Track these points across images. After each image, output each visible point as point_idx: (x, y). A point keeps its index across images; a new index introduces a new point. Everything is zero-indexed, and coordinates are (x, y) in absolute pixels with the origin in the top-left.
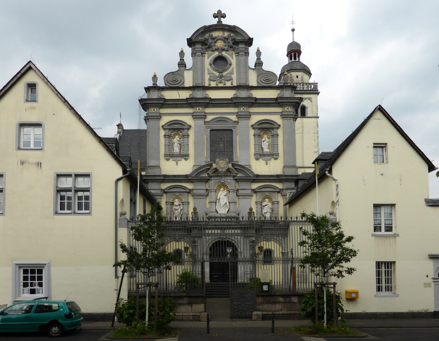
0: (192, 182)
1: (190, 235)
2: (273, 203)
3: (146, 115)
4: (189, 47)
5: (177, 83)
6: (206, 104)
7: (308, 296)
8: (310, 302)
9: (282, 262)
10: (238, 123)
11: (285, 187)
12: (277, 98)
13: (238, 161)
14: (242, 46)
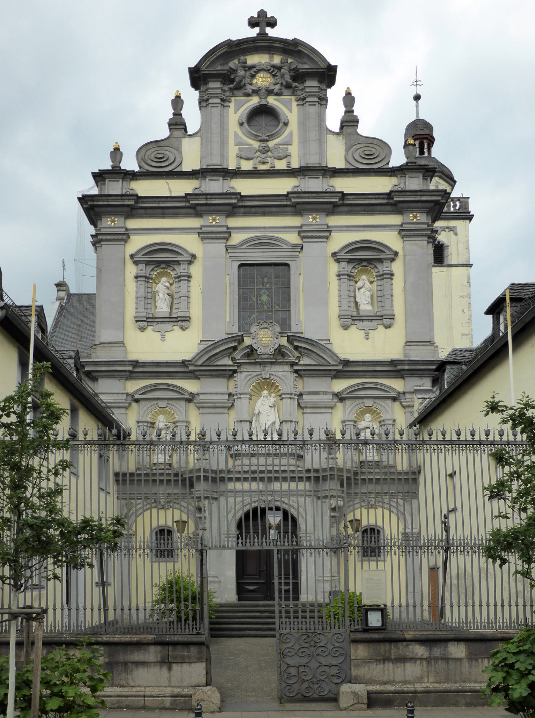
0: (197, 378)
1: (191, 493)
2: (383, 423)
3: (93, 232)
4: (193, 89)
5: (166, 164)
6: (230, 208)
8: (517, 666)
10: (302, 249)
11: (409, 388)
12: (391, 192)
13: (301, 331)
14: (312, 84)
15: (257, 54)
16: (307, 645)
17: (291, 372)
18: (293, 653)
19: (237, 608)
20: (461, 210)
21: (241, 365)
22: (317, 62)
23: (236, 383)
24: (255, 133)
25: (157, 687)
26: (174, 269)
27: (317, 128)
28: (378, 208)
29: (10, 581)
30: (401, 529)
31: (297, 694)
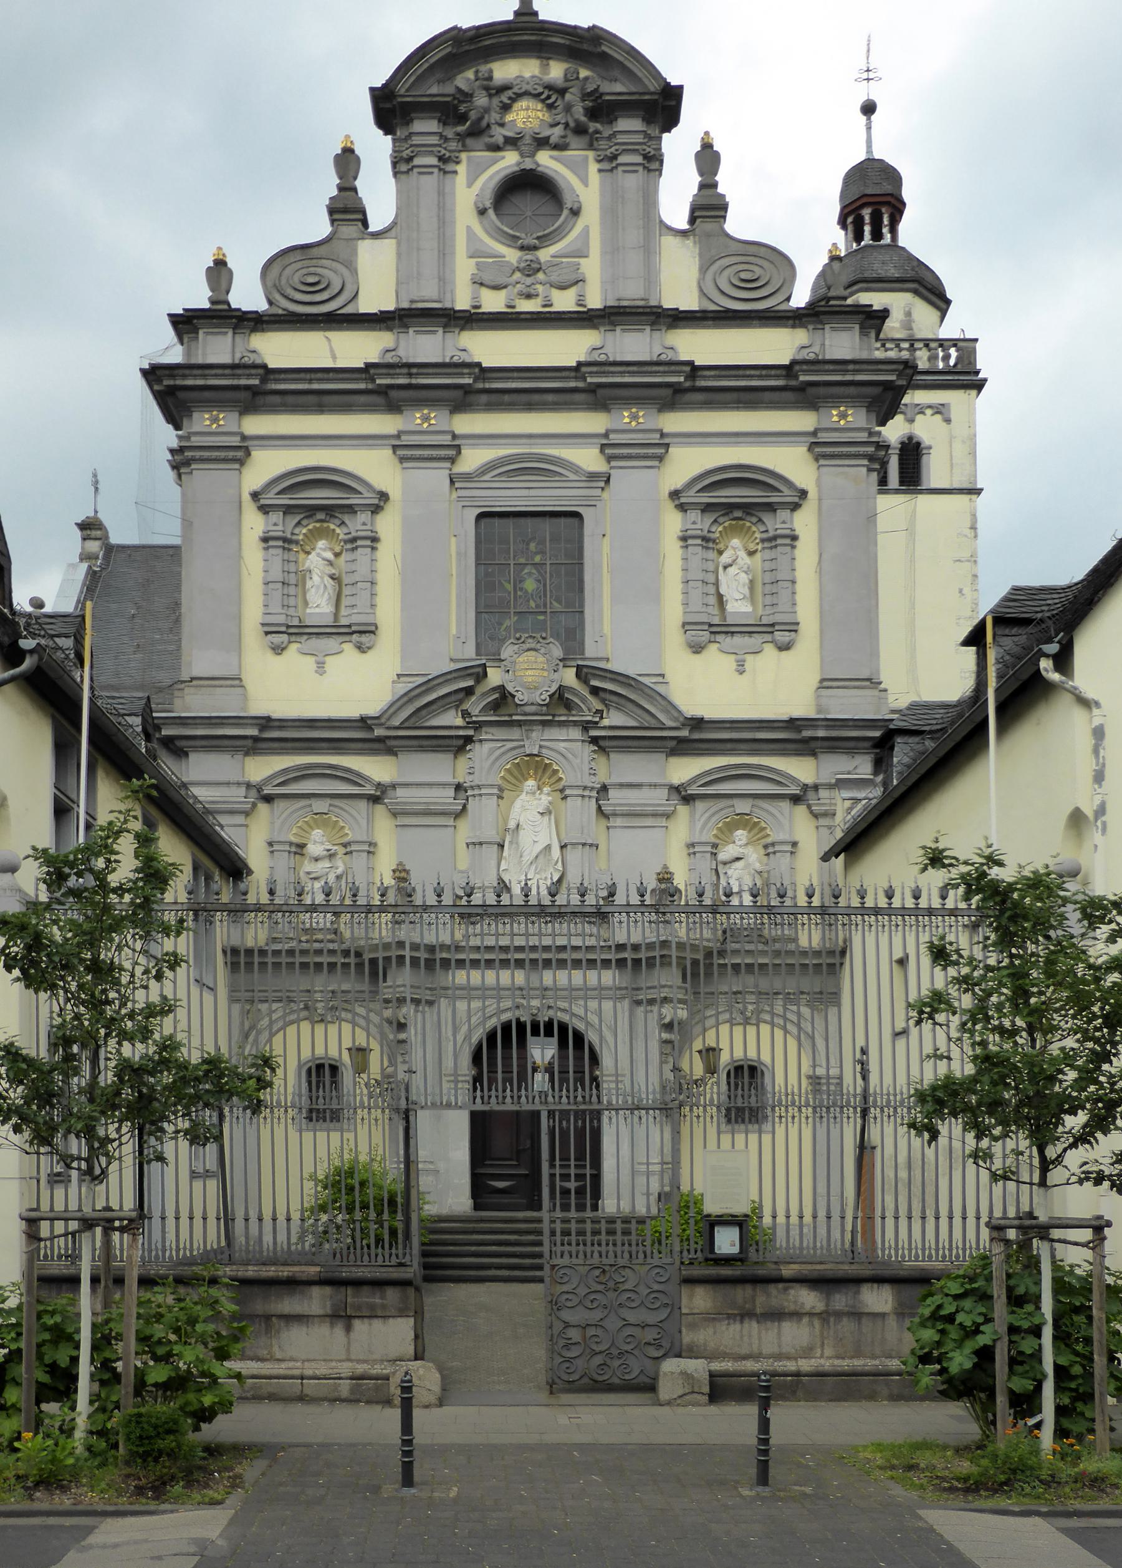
0: (391, 752)
2: (771, 850)
3: (175, 444)
4: (381, 132)
6: (458, 394)
7: (955, 1288)
8: (960, 1318)
9: (815, 1112)
10: (608, 481)
11: (826, 777)
12: (794, 363)
14: (629, 125)
15: (515, 57)
16: (600, 1287)
17: (583, 741)
18: (576, 1300)
19: (471, 1225)
20: (959, 366)
21: (480, 727)
22: (640, 80)
23: (471, 764)
24: (511, 232)
25: (324, 1360)
26: (343, 523)
27: (641, 222)
28: (767, 395)
29: (79, 1164)
30: (806, 1068)
31: (581, 1377)
